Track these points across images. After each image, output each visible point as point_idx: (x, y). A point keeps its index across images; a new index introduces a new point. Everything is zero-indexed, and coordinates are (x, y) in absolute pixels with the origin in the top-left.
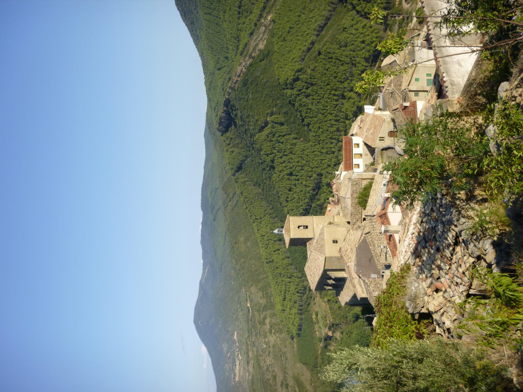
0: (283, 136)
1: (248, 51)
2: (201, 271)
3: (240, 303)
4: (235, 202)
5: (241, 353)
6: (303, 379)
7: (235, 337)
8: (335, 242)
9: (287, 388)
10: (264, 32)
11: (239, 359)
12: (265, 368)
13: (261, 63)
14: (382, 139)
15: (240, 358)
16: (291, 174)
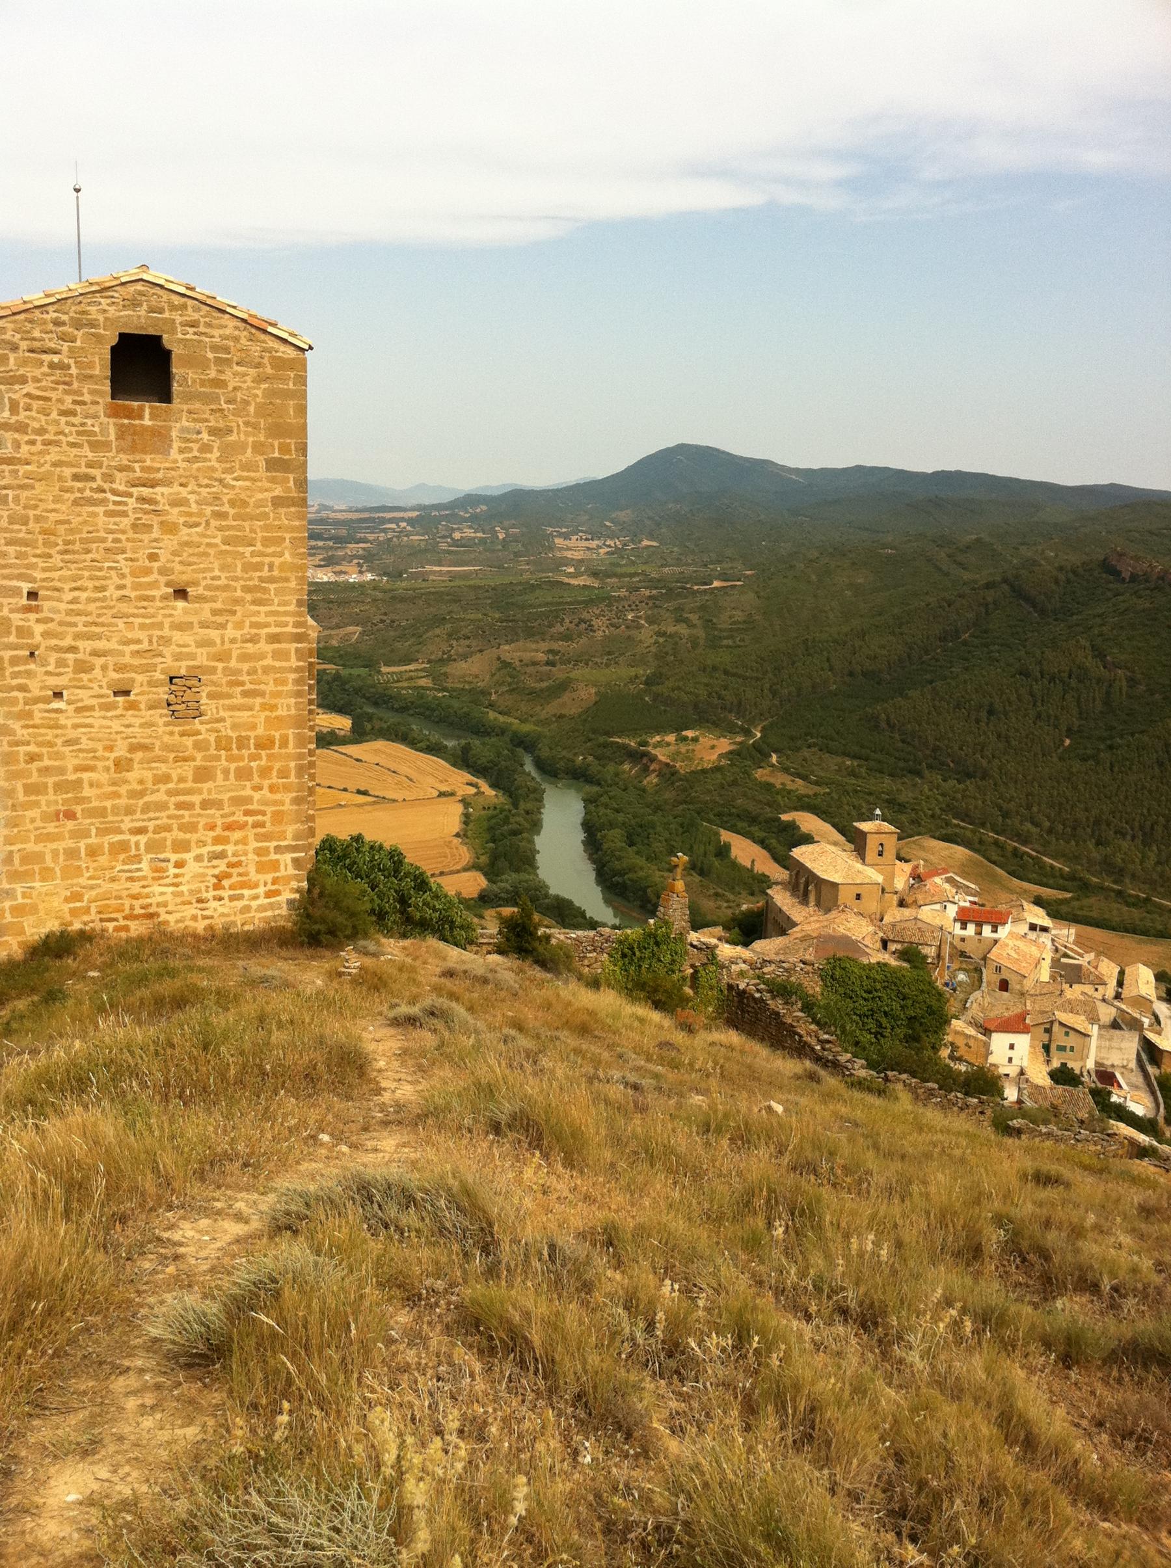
0: (1078, 701)
2: (792, 463)
4: (944, 568)
6: (566, 697)
7: (646, 543)
8: (858, 897)
9: (548, 663)
11: (599, 547)
12: (585, 615)
16: (991, 712)
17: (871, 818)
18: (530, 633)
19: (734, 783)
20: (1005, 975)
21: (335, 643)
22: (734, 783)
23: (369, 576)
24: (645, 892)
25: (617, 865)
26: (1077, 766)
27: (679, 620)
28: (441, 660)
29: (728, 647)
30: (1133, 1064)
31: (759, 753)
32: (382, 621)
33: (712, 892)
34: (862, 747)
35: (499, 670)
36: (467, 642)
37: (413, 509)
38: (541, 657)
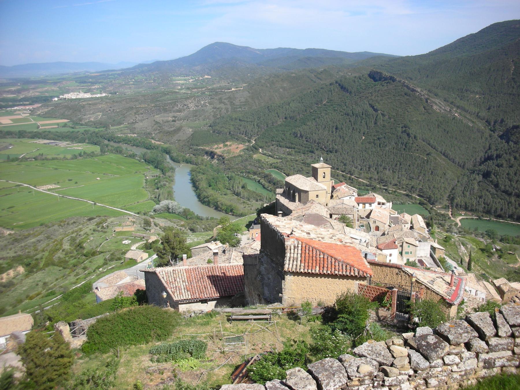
1: (432, 97)
3: (233, 82)
4: (314, 80)
5: (194, 81)
6: (180, 134)
7: (206, 77)
8: (317, 196)
10: (446, 110)
12: (186, 103)
13: (422, 107)
14: (375, 222)
15: (190, 81)
16: (336, 129)
17: (318, 161)
18: (165, 111)
19: (246, 160)
20: (378, 224)
21: (92, 119)
22: (246, 160)
23: (104, 95)
24: (217, 203)
25: (205, 194)
26: (368, 146)
27: (221, 102)
28: (133, 123)
29: (240, 111)
30: (429, 255)
31: (255, 149)
32: (110, 110)
33: (242, 201)
34: (292, 144)
35: (155, 124)
36: (142, 115)
37: (119, 70)
38: (170, 119)
